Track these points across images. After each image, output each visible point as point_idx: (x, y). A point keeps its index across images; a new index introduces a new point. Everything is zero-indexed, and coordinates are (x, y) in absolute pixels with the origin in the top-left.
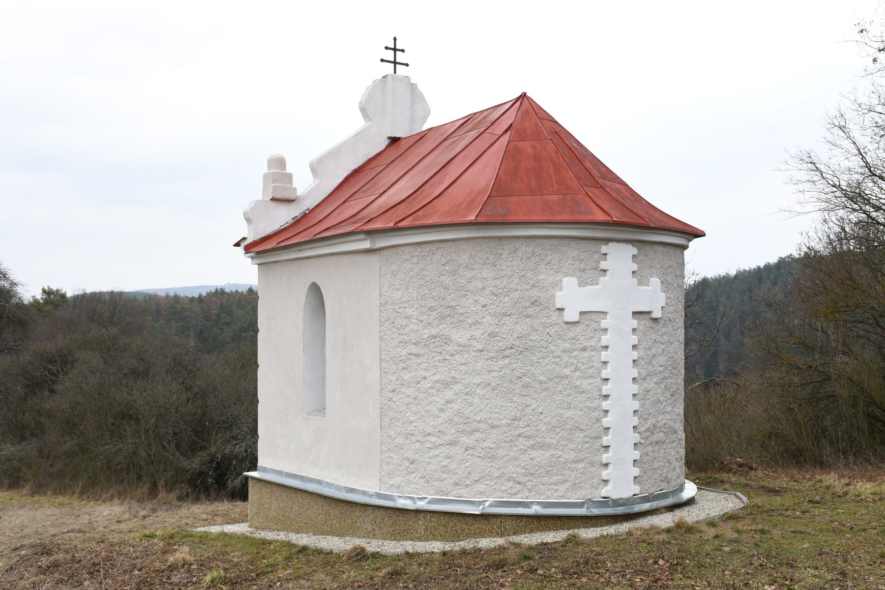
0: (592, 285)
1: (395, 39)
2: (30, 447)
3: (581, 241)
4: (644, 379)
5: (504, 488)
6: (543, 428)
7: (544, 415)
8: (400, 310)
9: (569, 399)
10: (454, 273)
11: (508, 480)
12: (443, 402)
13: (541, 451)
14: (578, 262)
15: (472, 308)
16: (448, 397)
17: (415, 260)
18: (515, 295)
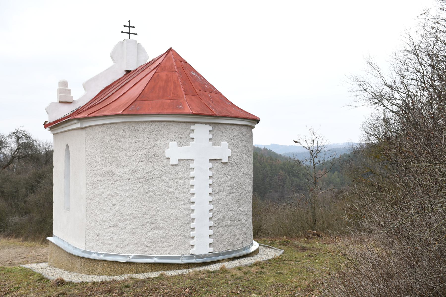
0: (185, 146)
1: (129, 21)
2: (26, 218)
3: (179, 123)
4: (217, 193)
5: (140, 249)
6: (159, 218)
7: (160, 212)
8: (94, 158)
9: (173, 204)
10: (116, 140)
11: (142, 245)
12: (111, 205)
13: (158, 230)
14: (178, 134)
15: (124, 158)
16: (113, 203)
17: (100, 133)
18: (145, 151)
